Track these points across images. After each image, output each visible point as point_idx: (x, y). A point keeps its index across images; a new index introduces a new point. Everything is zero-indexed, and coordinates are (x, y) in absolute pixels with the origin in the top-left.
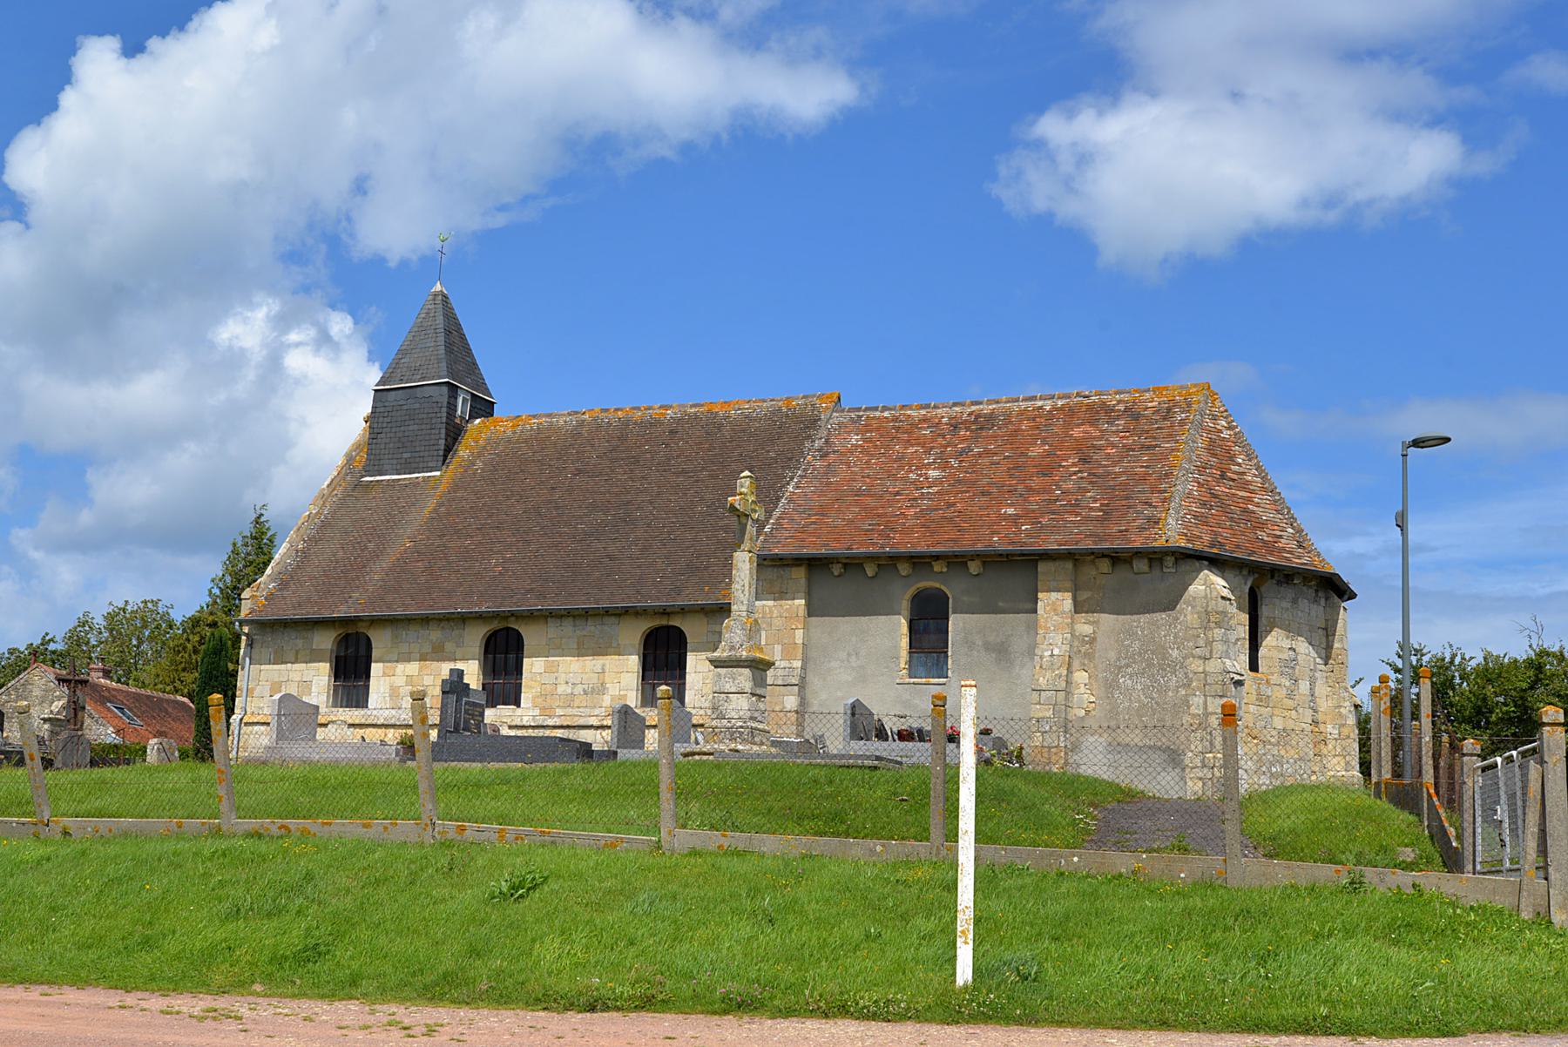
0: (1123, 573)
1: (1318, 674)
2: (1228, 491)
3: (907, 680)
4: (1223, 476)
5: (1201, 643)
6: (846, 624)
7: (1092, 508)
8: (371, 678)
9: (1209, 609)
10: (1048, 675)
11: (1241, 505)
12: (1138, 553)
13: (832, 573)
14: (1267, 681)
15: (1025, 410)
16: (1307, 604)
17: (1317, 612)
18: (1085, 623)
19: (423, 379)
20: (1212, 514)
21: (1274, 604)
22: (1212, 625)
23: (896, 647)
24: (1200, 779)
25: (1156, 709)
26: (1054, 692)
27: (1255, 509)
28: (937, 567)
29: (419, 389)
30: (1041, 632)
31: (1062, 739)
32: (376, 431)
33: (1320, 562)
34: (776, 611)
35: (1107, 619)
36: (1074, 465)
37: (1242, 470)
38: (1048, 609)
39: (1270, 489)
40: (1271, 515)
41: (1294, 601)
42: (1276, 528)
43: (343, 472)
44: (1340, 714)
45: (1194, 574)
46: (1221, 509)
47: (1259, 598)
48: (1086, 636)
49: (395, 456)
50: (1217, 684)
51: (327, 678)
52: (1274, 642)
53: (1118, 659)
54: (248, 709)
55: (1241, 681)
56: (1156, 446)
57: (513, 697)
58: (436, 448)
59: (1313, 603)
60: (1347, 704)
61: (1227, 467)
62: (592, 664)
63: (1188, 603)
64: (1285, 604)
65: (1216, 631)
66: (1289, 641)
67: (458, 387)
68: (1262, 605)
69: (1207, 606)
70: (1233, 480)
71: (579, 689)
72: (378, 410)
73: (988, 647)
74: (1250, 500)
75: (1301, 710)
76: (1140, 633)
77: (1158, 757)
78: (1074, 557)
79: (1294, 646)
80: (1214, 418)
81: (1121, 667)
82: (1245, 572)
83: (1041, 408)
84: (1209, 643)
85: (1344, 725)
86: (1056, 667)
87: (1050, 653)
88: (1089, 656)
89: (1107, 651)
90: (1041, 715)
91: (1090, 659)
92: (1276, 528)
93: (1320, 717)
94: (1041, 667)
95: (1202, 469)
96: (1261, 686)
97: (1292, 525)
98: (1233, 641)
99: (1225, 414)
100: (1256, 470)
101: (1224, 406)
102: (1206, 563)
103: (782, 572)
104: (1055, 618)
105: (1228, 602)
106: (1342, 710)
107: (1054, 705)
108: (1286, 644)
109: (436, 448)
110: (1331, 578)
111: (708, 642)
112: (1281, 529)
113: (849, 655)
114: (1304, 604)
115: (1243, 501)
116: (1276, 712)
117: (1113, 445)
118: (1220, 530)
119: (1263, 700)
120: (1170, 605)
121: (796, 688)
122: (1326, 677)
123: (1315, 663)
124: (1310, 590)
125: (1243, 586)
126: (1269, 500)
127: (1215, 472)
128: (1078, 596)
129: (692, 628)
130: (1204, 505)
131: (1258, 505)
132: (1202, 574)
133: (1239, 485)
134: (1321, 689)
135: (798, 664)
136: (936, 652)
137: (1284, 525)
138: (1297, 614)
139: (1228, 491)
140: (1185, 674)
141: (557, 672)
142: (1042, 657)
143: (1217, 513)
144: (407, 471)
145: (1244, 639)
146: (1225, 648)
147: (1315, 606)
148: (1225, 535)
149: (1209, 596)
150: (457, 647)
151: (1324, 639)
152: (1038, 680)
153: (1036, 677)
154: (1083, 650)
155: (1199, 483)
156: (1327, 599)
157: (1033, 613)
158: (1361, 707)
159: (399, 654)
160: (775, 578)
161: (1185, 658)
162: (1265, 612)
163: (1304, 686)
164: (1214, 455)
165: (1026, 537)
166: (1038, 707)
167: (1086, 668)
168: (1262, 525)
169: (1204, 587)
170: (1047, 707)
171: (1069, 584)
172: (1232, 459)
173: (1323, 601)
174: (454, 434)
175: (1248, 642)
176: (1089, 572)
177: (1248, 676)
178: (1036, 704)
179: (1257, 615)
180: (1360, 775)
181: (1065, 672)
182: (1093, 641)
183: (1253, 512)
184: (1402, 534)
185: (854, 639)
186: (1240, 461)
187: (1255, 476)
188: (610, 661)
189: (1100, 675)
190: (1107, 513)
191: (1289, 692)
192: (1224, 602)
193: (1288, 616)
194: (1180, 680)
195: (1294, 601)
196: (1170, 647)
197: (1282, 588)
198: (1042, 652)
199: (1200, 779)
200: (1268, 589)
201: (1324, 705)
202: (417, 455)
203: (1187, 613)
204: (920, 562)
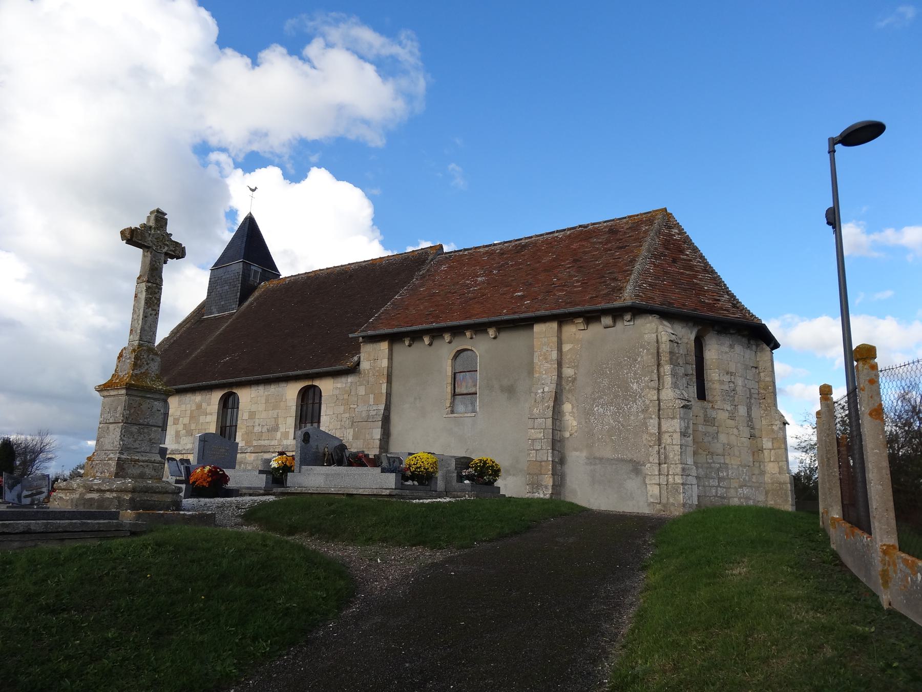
7: (575, 286)
15: (547, 239)
18: (568, 367)
19: (223, 264)
20: (664, 284)
27: (698, 282)
36: (569, 263)
41: (731, 347)
42: (715, 294)
44: (773, 430)
48: (570, 377)
53: (593, 393)
55: (688, 405)
56: (626, 246)
66: (729, 376)
71: (265, 430)
79: (733, 380)
83: (557, 237)
90: (535, 437)
92: (715, 294)
94: (535, 401)
104: (546, 365)
107: (544, 429)
113: (415, 399)
117: (598, 249)
130: (657, 278)
131: (701, 280)
137: (722, 293)
141: (255, 418)
145: (692, 374)
148: (674, 297)
150: (208, 405)
155: (655, 264)
160: (371, 350)
163: (742, 410)
164: (667, 249)
172: (682, 251)
175: (695, 377)
183: (697, 284)
184: (835, 232)
186: (688, 253)
187: (700, 262)
195: (731, 347)
196: (631, 382)
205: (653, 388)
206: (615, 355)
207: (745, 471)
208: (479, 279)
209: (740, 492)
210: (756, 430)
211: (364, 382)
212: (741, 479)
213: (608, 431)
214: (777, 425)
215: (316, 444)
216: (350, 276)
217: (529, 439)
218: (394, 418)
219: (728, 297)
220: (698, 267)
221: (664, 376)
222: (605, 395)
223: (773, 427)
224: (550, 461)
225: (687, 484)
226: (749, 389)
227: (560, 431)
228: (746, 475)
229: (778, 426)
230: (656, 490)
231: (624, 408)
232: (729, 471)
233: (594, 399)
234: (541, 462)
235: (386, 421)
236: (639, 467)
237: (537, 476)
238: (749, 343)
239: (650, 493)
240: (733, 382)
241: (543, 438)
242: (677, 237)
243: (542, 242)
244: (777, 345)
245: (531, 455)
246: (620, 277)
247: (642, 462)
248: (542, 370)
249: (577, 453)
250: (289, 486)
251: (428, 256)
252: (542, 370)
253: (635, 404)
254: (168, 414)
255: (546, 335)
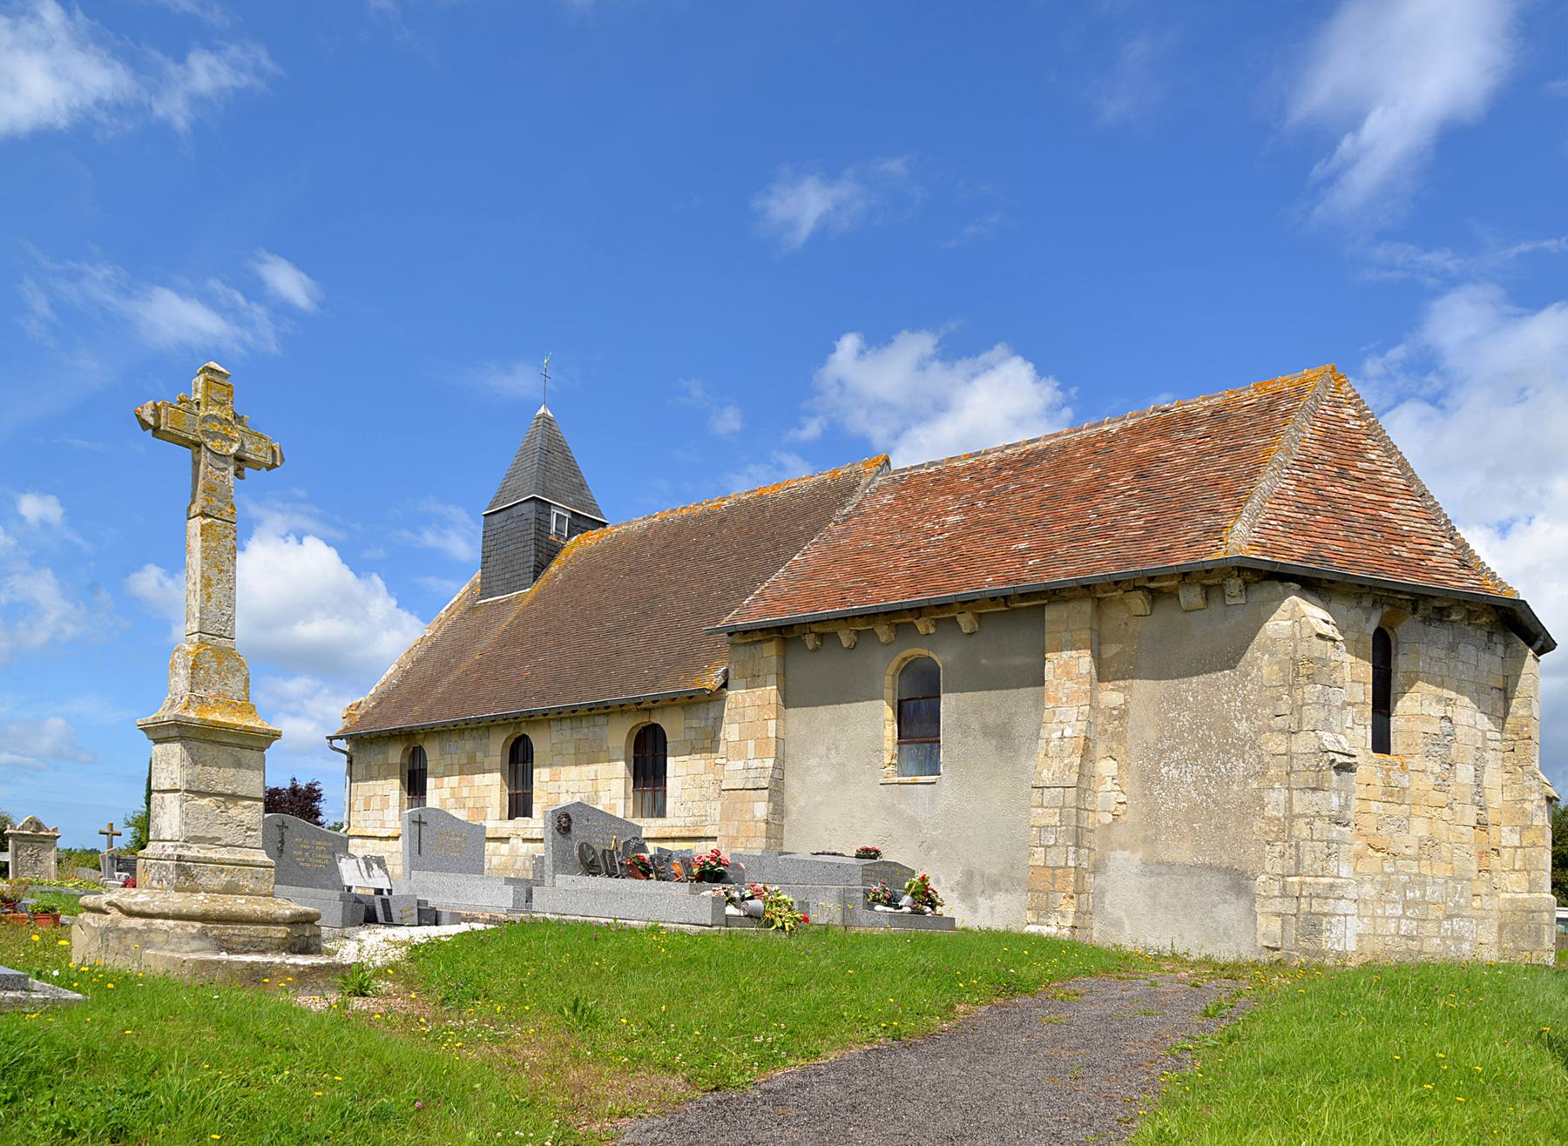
0: (1166, 614)
1: (1489, 755)
2: (1347, 492)
3: (897, 779)
4: (1342, 474)
5: (1283, 708)
6: (825, 714)
7: (1131, 528)
8: (428, 792)
9: (1298, 656)
10: (1055, 765)
11: (1369, 511)
12: (1185, 576)
13: (807, 647)
14: (1402, 765)
16: (1474, 653)
17: (1490, 664)
19: (518, 498)
21: (1417, 653)
22: (1303, 680)
23: (879, 737)
24: (1279, 915)
25: (1213, 811)
26: (1062, 790)
27: (1392, 516)
28: (922, 626)
29: (515, 508)
30: (1049, 705)
31: (1071, 856)
32: (486, 554)
33: (1496, 586)
34: (748, 699)
35: (1143, 688)
37: (1374, 467)
38: (1058, 671)
39: (1420, 493)
40: (1419, 525)
41: (1452, 648)
42: (1424, 541)
43: (465, 596)
44: (1524, 812)
45: (1277, 603)
46: (1333, 515)
47: (1393, 645)
48: (1114, 709)
49: (500, 578)
50: (1308, 770)
51: (398, 792)
52: (1411, 707)
54: (352, 824)
57: (660, 812)
58: (528, 564)
59: (1484, 650)
60: (1536, 796)
61: (1351, 463)
62: (588, 770)
63: (1264, 649)
64: (1436, 652)
65: (1309, 688)
66: (1441, 707)
67: (550, 504)
68: (1397, 654)
69: (1295, 651)
70: (1359, 480)
72: (487, 534)
73: (986, 731)
74: (1384, 505)
75: (1458, 808)
76: (1191, 699)
77: (1216, 882)
78: (1087, 591)
79: (1449, 715)
80: (1338, 405)
81: (1163, 751)
82: (1367, 603)
83: (1106, 432)
84: (1297, 708)
85: (1528, 827)
86: (1066, 753)
87: (1059, 734)
88: (1119, 737)
89: (1144, 729)
90: (1044, 822)
91: (1119, 741)
92: (1424, 541)
93: (1490, 817)
95: (1306, 464)
96: (1391, 773)
97: (1451, 538)
98: (1339, 704)
99: (1354, 401)
100: (1399, 468)
101: (1354, 390)
102: (1296, 586)
103: (753, 650)
104: (1069, 684)
105: (1330, 644)
106: (1527, 805)
107: (1061, 808)
108: (1437, 710)
109: (528, 564)
110: (1514, 611)
111: (685, 740)
112: (1433, 543)
113: (829, 749)
114: (1468, 651)
115: (1371, 506)
116: (1416, 810)
117: (1185, 454)
118: (1327, 541)
119: (1392, 793)
120: (1229, 656)
121: (766, 792)
122: (1503, 759)
123: (1485, 739)
124: (1479, 632)
125: (1363, 624)
126: (1417, 506)
127: (1329, 468)
128: (1103, 652)
129: (673, 726)
130: (1304, 508)
131: (1397, 511)
132: (1286, 601)
133: (1367, 486)
134: (1494, 776)
135: (770, 763)
136: (928, 742)
138: (1456, 666)
139: (1347, 492)
140: (1259, 757)
142: (1048, 742)
143: (1325, 520)
144: (509, 590)
146: (1323, 714)
147: (1487, 656)
149: (1298, 635)
150: (485, 756)
151: (1501, 705)
152: (1040, 773)
153: (1039, 769)
154: (1110, 728)
156: (1507, 646)
157: (1039, 686)
158: (1558, 800)
159: (445, 766)
160: (747, 659)
161: (1259, 732)
162: (1402, 664)
163: (1465, 773)
164: (1332, 448)
165: (1034, 573)
166: (1040, 811)
167: (1114, 755)
168: (1402, 538)
169: (1290, 623)
170: (1051, 811)
171: (1085, 635)
172: (1360, 454)
173: (1500, 649)
174: (547, 553)
176: (1117, 616)
177: (1366, 758)
178: (1037, 807)
179: (1391, 670)
180: (1552, 897)
181: (1079, 760)
182: (1123, 714)
183: (1388, 520)
185: (833, 729)
186: (1373, 457)
188: (601, 768)
189: (1134, 764)
190: (1150, 531)
191: (1440, 782)
192: (1323, 642)
193: (1441, 669)
194: (1249, 766)
195: (1452, 648)
197: (1431, 628)
198: (1050, 734)
199: (1279, 915)
200: (1407, 632)
201: (1496, 799)
202: (514, 573)
203: (1262, 664)
204: (900, 618)
205: (1279, 731)
206: (1205, 664)
207: (1459, 889)
208: (951, 519)
209: (1447, 926)
210: (1490, 810)
211: (737, 718)
212: (1451, 904)
213: (1187, 813)
214: (1532, 802)
215: (39, 894)
216: (722, 521)
217: (1033, 826)
218: (792, 784)
219: (1451, 546)
220: (1392, 485)
221: (1302, 706)
222: (1183, 743)
223: (1525, 806)
224: (1070, 867)
225: (1336, 914)
226: (1482, 731)
227: (1093, 811)
228: (1461, 897)
229: (1535, 803)
230: (1275, 925)
231: (1219, 768)
232: (1428, 888)
233: (1162, 752)
234: (1054, 868)
235: (776, 790)
236: (1244, 882)
237: (1047, 894)
238: (1490, 640)
239: (1262, 930)
240: (1449, 718)
241: (1059, 824)
242: (1353, 424)
243: (1079, 443)
244: (1539, 640)
245: (1036, 856)
246: (1223, 506)
247: (1249, 873)
248: (1060, 695)
249: (1127, 853)
250: (536, 910)
251: (861, 478)
252: (1060, 695)
253: (1241, 761)
254: (426, 769)
255: (1068, 626)
